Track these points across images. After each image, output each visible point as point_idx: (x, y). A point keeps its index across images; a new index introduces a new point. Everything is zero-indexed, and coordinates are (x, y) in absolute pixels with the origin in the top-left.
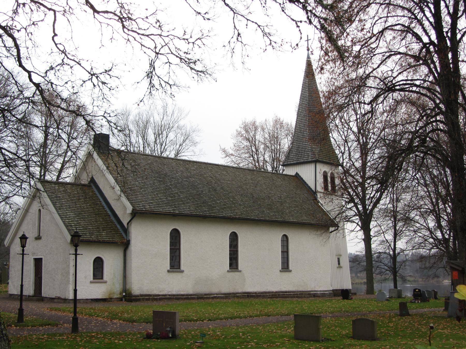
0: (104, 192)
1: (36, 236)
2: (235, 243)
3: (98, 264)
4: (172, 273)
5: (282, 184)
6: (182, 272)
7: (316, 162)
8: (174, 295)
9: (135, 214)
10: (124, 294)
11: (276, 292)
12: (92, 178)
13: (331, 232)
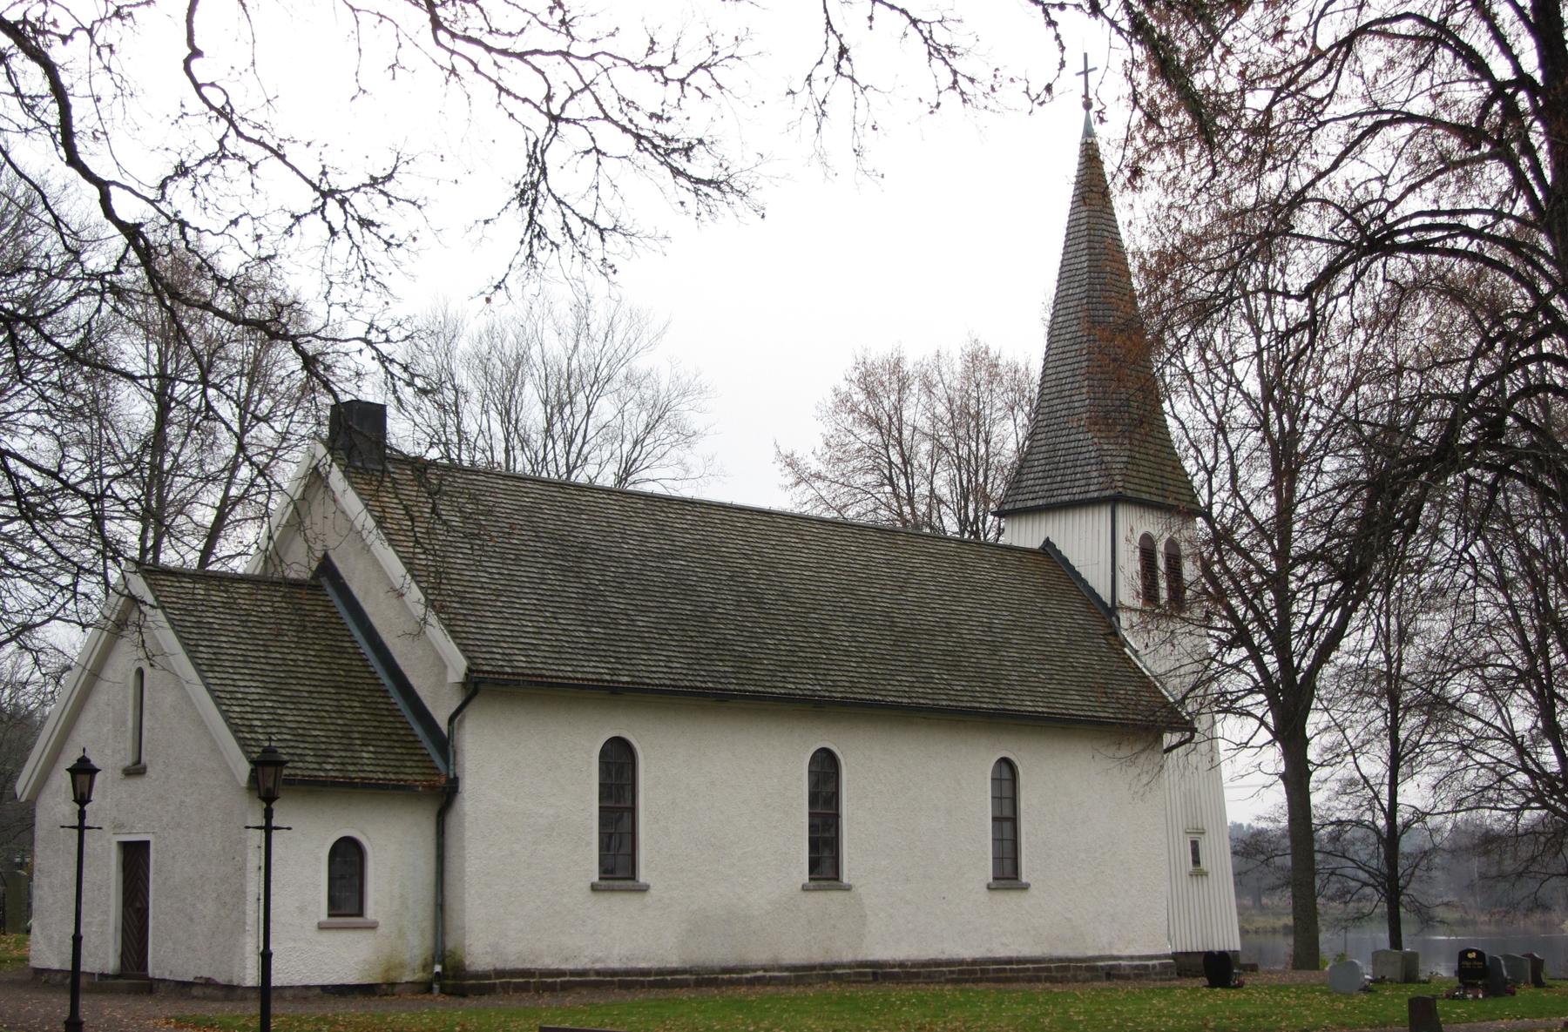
0: (368, 607)
1: (128, 762)
2: (830, 788)
3: (347, 861)
4: (607, 895)
5: (995, 580)
6: (644, 889)
7: (1114, 501)
8: (614, 973)
9: (476, 687)
10: (438, 968)
11: (975, 962)
12: (326, 557)
13: (1170, 749)
